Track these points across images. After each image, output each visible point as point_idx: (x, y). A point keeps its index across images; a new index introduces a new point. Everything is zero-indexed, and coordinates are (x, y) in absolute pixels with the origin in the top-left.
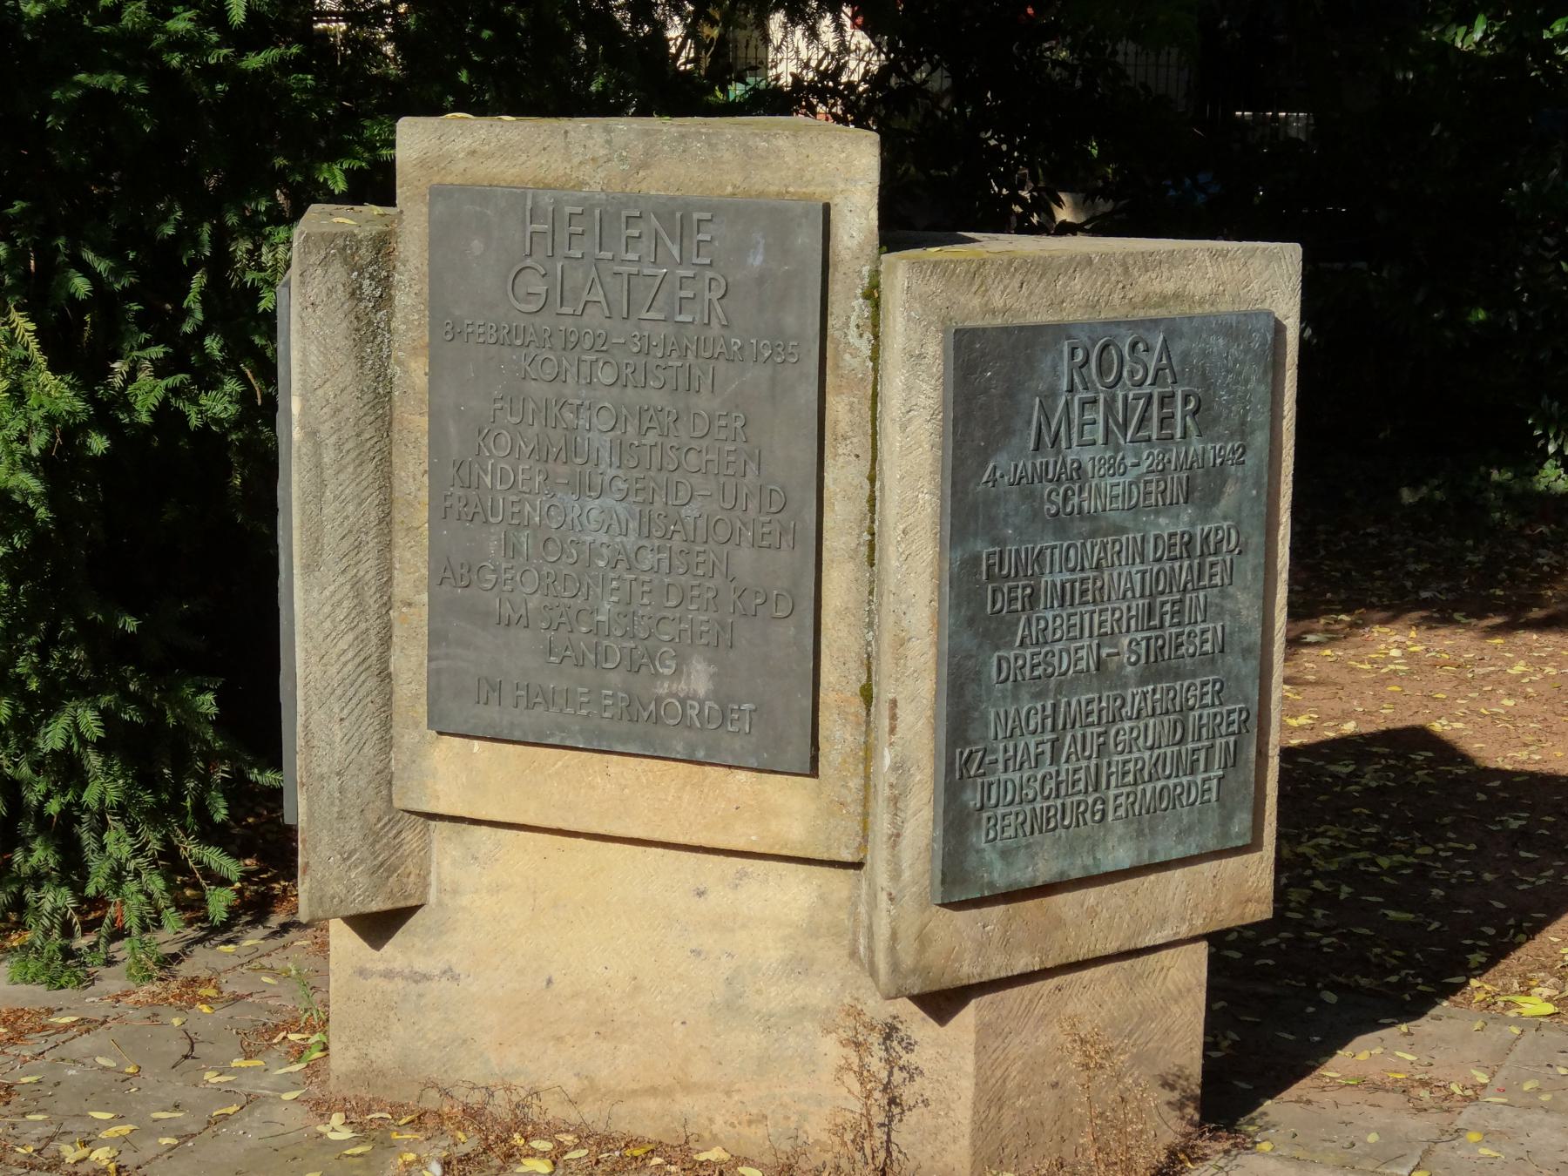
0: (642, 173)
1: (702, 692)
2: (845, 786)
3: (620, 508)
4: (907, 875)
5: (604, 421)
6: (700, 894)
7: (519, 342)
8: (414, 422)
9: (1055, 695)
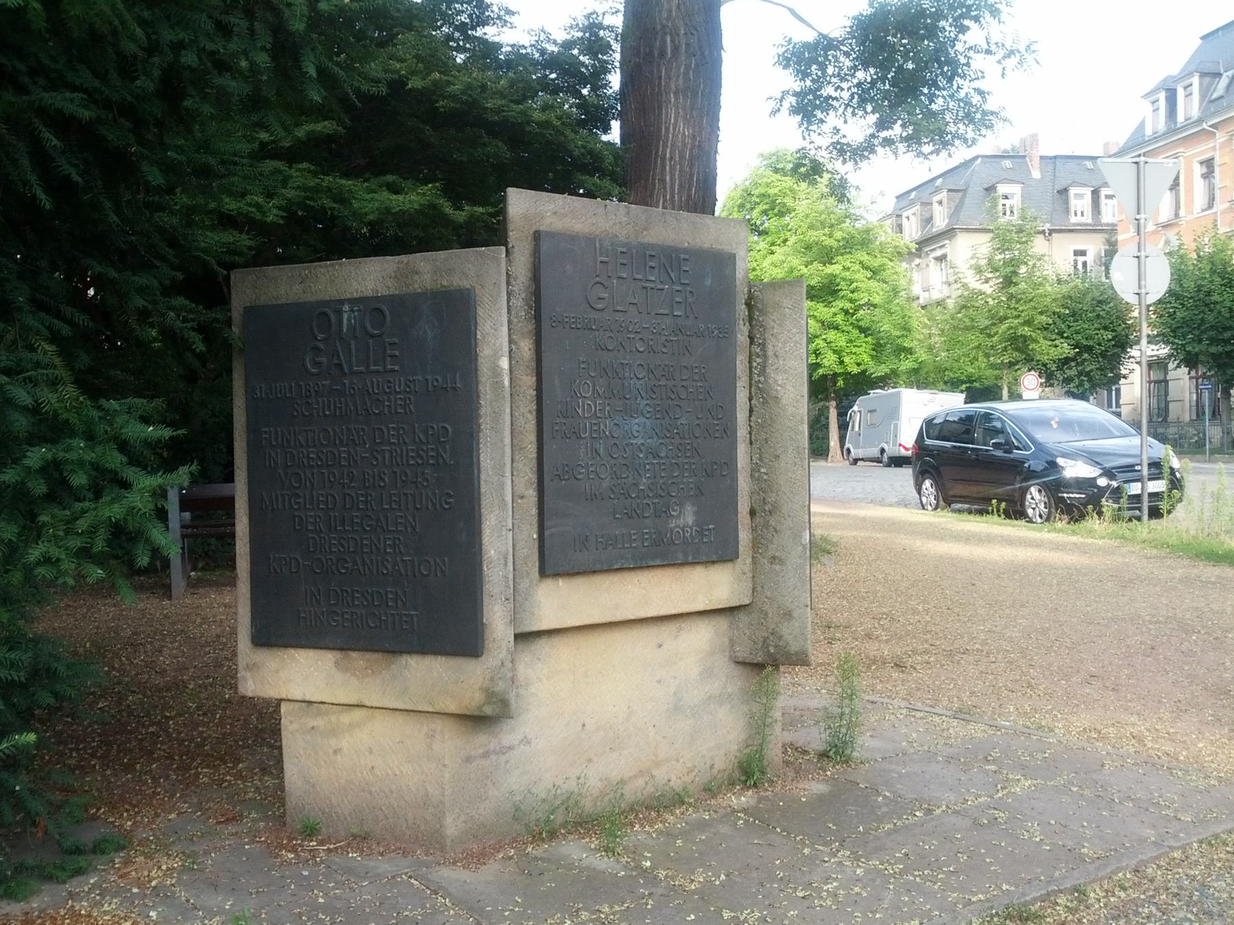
0: (645, 233)
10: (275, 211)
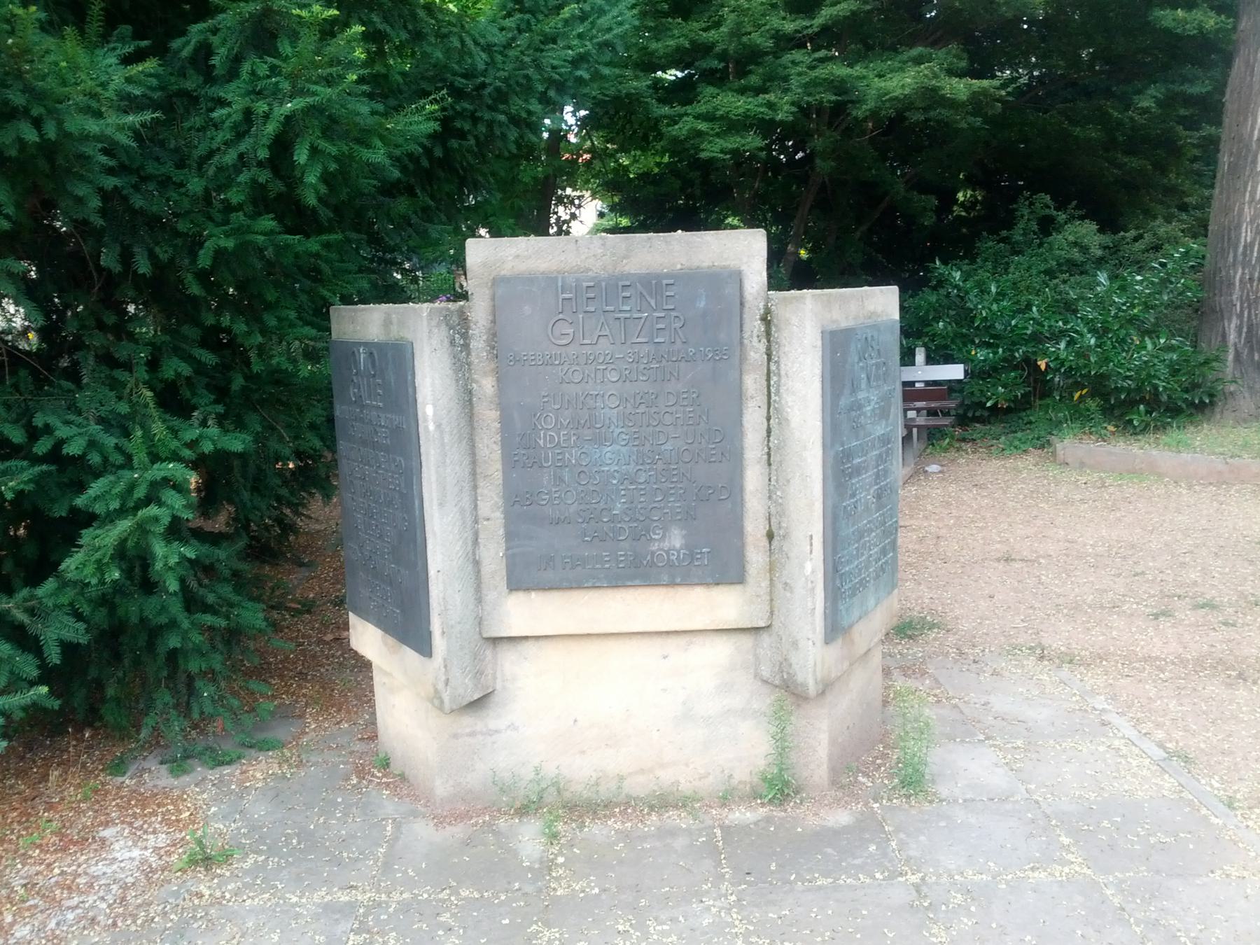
1: (678, 545)
3: (624, 450)
4: (818, 629)
5: (614, 402)
7: (557, 362)
8: (489, 416)
10: (786, 108)
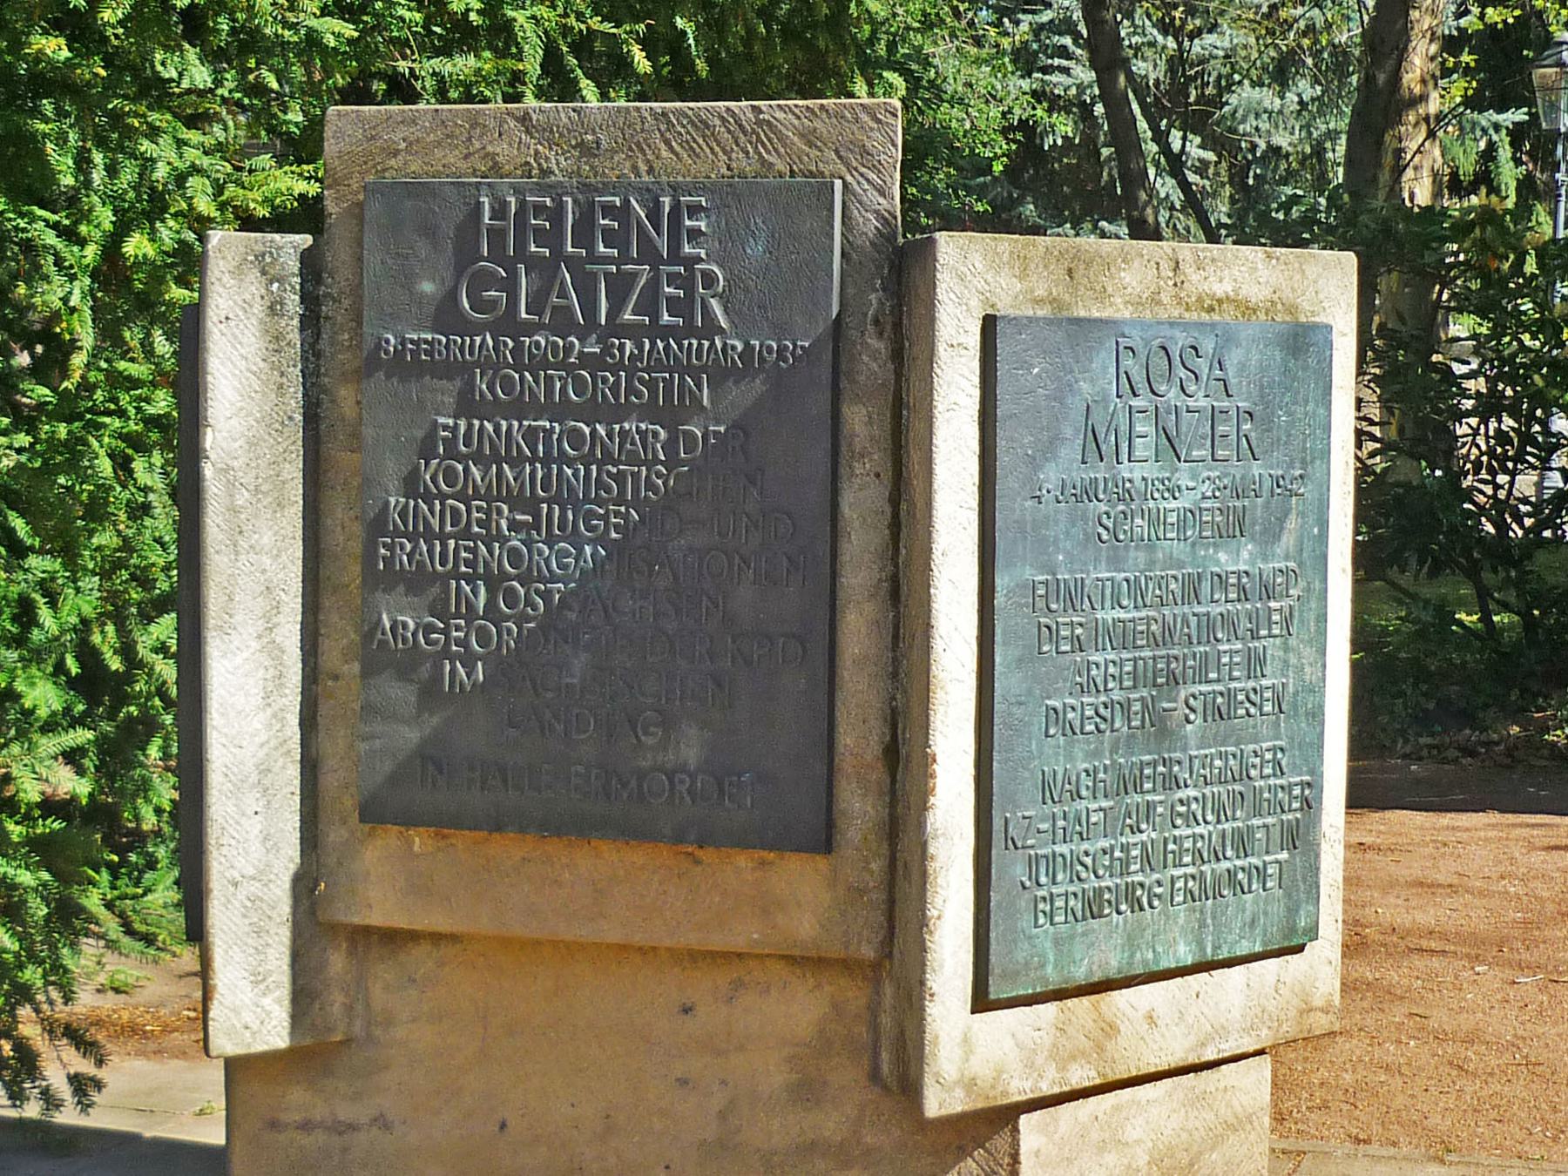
2: (866, 868)
6: (686, 1010)
9: (1111, 755)
